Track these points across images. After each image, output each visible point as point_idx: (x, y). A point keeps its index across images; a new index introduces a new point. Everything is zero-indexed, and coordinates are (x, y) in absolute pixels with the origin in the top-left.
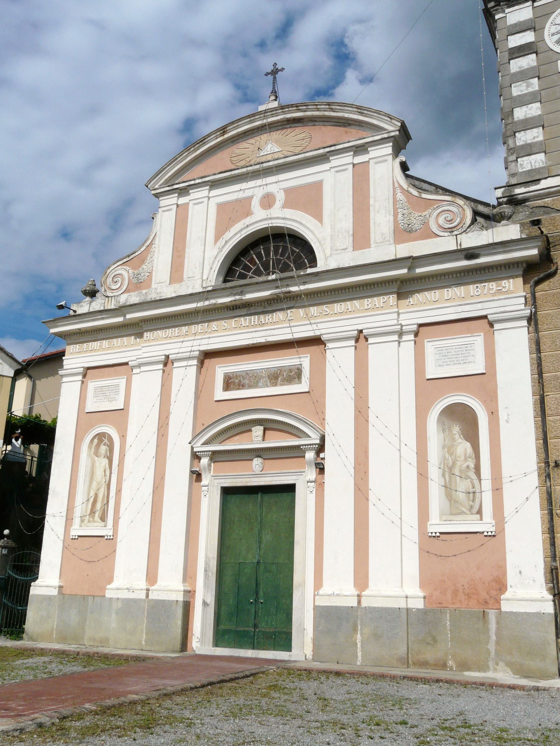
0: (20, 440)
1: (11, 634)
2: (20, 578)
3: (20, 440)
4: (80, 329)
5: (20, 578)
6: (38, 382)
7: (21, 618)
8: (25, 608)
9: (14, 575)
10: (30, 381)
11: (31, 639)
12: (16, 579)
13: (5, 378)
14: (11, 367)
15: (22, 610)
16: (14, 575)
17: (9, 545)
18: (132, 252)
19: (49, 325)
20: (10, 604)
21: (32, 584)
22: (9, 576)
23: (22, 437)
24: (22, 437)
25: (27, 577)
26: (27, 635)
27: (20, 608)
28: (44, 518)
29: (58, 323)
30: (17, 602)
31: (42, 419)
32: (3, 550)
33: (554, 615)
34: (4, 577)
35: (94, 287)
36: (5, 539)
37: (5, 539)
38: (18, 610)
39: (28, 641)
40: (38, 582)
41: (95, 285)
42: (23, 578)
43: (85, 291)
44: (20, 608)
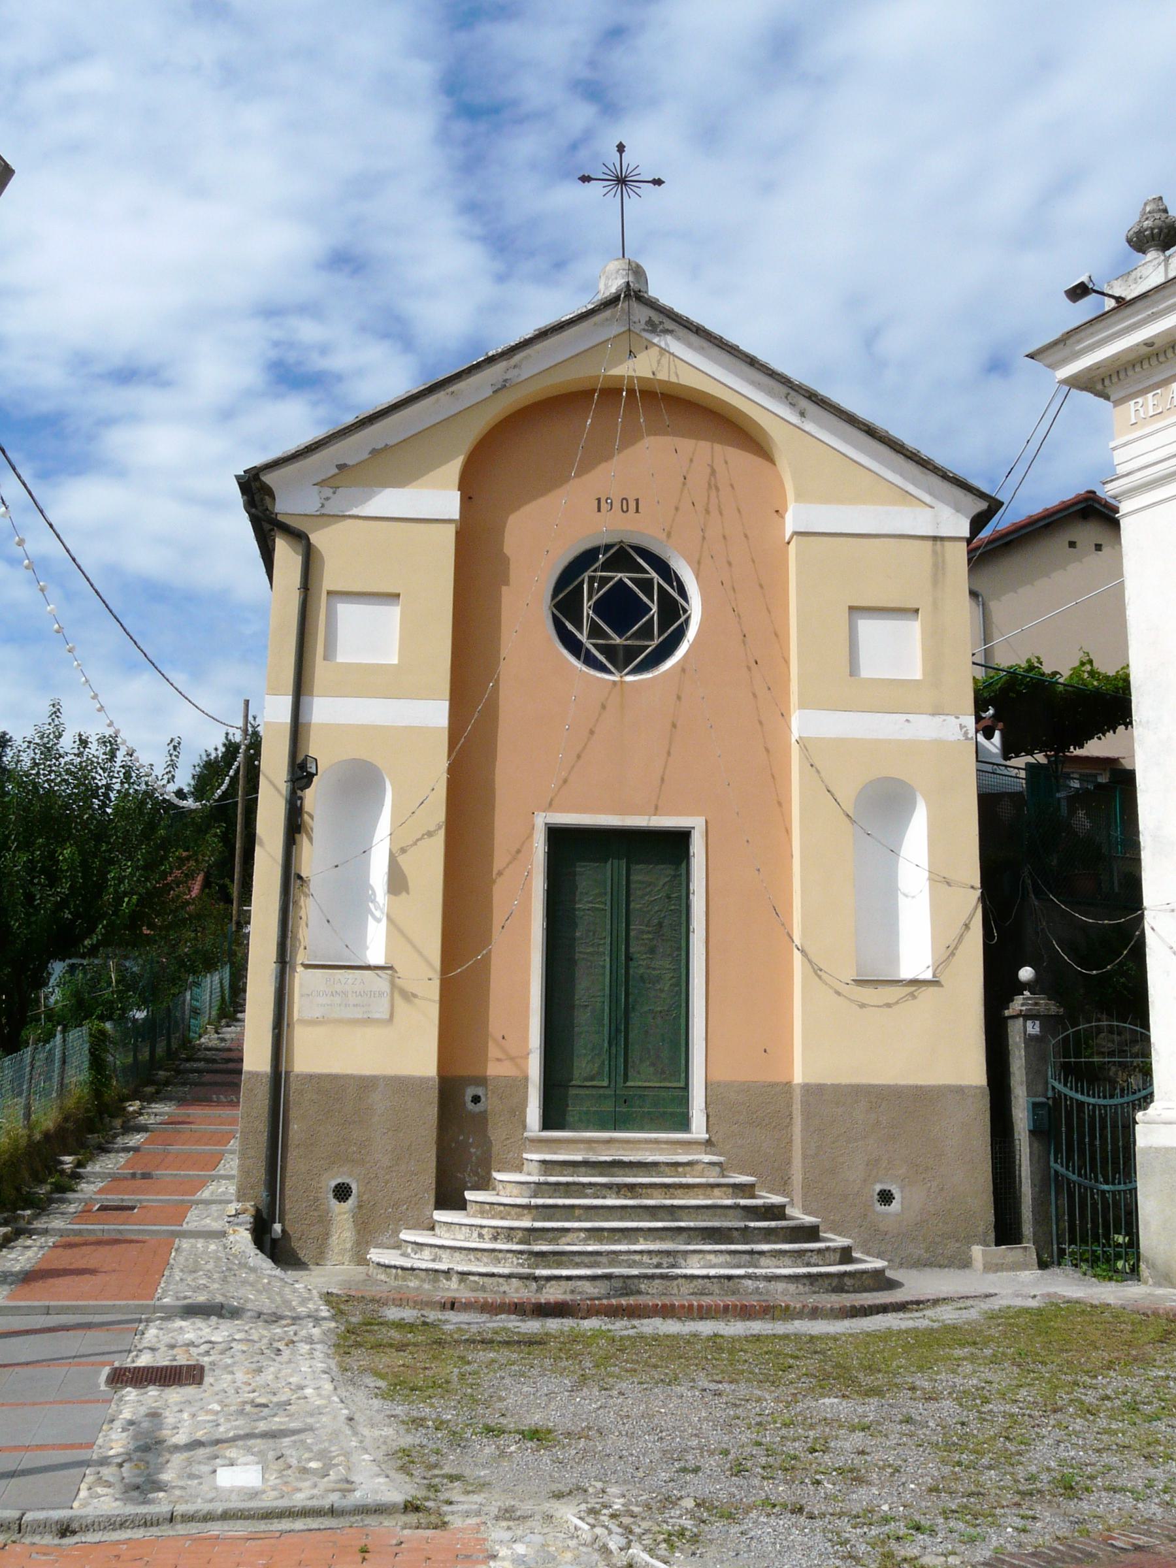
0: (997, 734)
1: (1094, 1261)
2: (1092, 1100)
3: (997, 734)
4: (1148, 344)
5: (1092, 1100)
6: (993, 605)
7: (1128, 1219)
8: (1130, 1186)
9: (1072, 1094)
10: (974, 604)
11: (1165, 1279)
12: (1081, 1104)
13: (947, 544)
14: (958, 511)
15: (1113, 1192)
16: (1072, 1094)
17: (1042, 1009)
18: (846, 819)
19: (1050, 360)
20: (1075, 1177)
21: (1139, 1116)
22: (1058, 1098)
23: (1001, 725)
24: (1001, 725)
25: (1112, 1097)
26: (1152, 1266)
27: (1106, 1187)
28: (1141, 918)
29: (1079, 342)
30: (1093, 1169)
31: (1047, 669)
32: (1029, 1023)
33: (434, 1095)
34: (1044, 1100)
35: (1164, 216)
36: (1027, 993)
37: (1027, 993)
38: (1103, 1192)
39: (1159, 1284)
40: (1154, 1110)
41: (1165, 211)
42: (1102, 1102)
43: (1139, 233)
44: (1106, 1187)
